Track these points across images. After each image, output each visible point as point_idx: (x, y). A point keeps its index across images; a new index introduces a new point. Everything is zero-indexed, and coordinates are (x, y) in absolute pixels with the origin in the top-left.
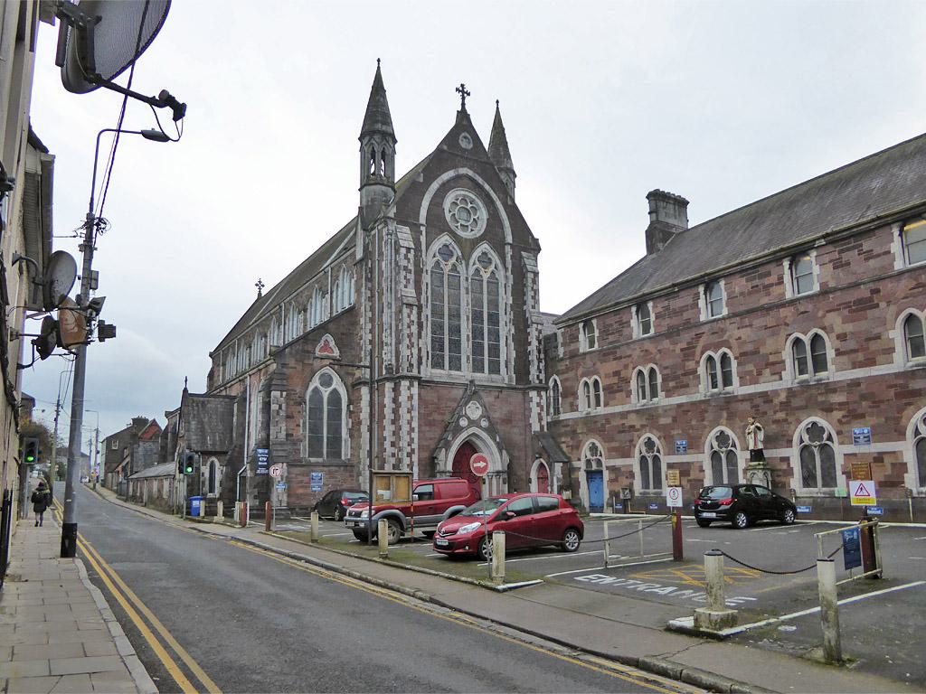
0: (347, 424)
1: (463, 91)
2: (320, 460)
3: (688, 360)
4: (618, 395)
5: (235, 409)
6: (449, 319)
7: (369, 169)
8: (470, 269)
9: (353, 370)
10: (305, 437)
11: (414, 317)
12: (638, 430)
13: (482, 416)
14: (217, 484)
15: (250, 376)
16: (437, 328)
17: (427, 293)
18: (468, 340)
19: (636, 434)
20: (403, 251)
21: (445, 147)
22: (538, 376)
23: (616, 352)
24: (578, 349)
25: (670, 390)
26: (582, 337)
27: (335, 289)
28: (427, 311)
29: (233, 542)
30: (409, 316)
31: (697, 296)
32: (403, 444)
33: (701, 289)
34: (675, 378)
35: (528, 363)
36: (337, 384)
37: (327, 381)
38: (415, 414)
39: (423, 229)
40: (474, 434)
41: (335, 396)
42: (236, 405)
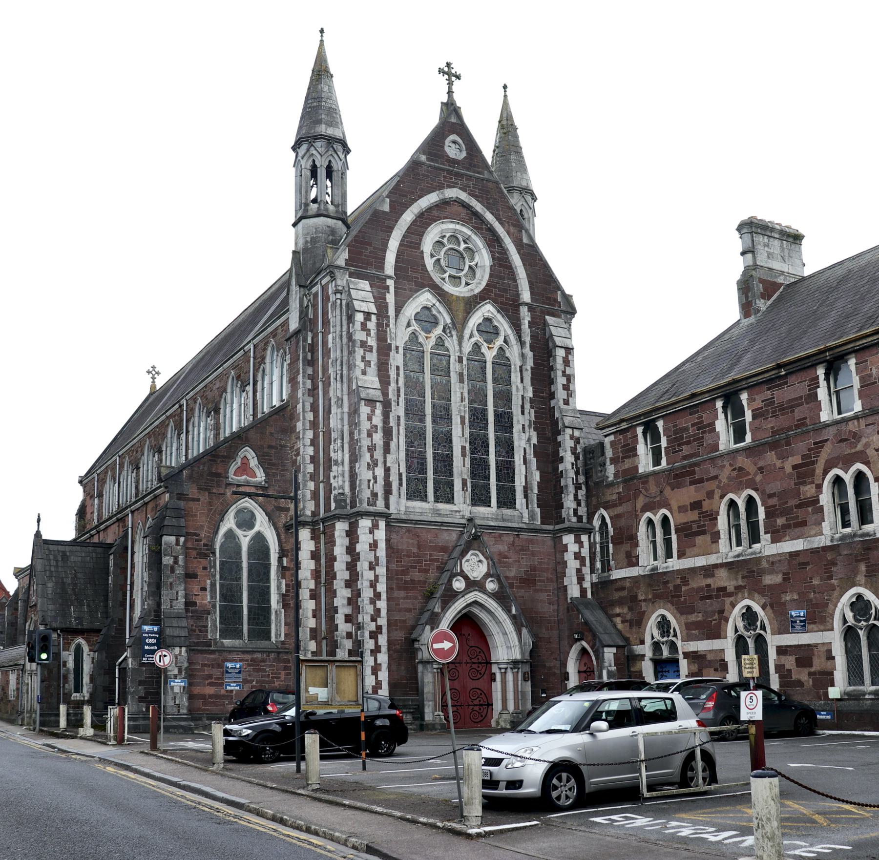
0: (279, 587)
1: (449, 73)
2: (237, 643)
3: (804, 483)
4: (699, 540)
5: (111, 563)
6: (434, 422)
7: (308, 192)
8: (464, 345)
9: (287, 503)
10: (214, 606)
11: (378, 420)
12: (730, 595)
13: (488, 575)
14: (86, 679)
15: (132, 512)
16: (415, 437)
17: (398, 381)
18: (464, 455)
19: (728, 600)
20: (359, 317)
21: (423, 158)
22: (576, 511)
23: (694, 472)
24: (637, 467)
25: (778, 531)
26: (643, 450)
27: (259, 378)
28: (399, 410)
29: (100, 766)
30: (370, 419)
31: (815, 380)
32: (365, 617)
33: (821, 372)
34: (785, 512)
35: (559, 491)
36: (262, 524)
37: (247, 521)
38: (382, 570)
39: (390, 283)
40: (475, 603)
41: (259, 546)
42: (112, 557)
